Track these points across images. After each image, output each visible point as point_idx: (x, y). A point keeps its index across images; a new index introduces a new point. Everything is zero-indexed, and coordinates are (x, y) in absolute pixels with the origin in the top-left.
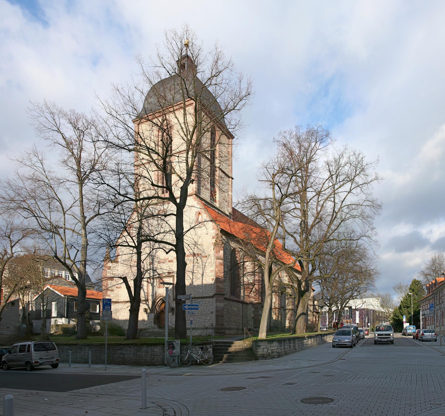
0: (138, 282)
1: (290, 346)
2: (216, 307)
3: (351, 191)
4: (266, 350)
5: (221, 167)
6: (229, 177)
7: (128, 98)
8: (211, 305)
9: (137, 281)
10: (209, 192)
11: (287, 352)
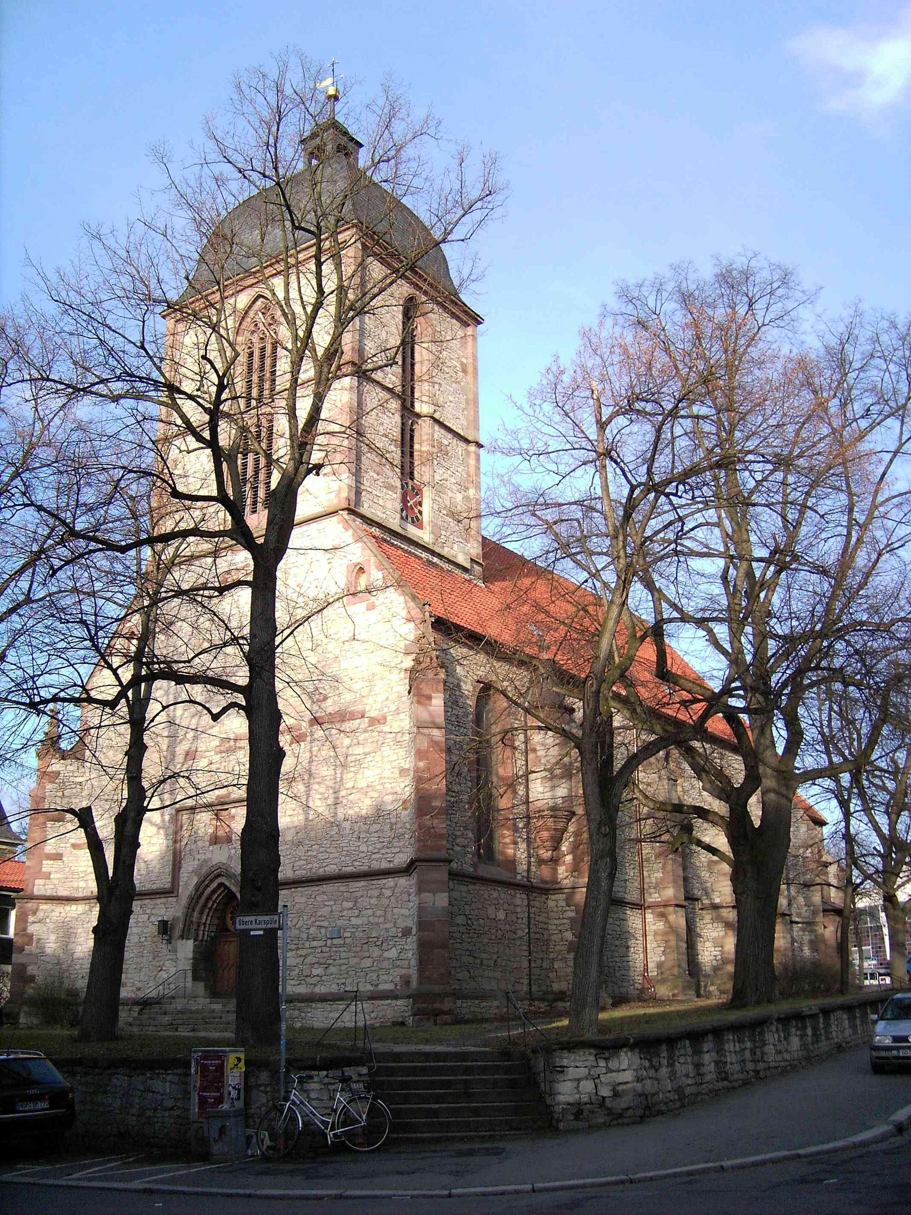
0: (129, 827)
1: (698, 1066)
2: (421, 909)
3: (902, 445)
4: (587, 1086)
5: (436, 416)
6: (467, 441)
7: (125, 254)
8: (398, 907)
9: (125, 821)
10: (398, 496)
11: (688, 1091)
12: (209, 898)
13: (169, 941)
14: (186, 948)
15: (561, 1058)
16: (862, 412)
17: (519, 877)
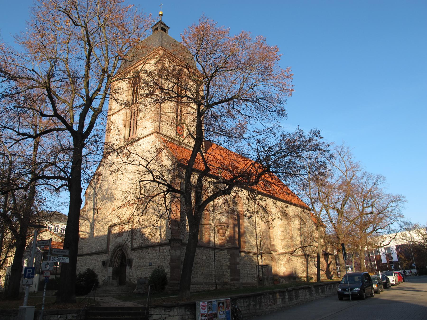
12: (117, 254)
13: (106, 268)
14: (110, 270)
15: (151, 311)
16: (400, 228)
17: (211, 245)
